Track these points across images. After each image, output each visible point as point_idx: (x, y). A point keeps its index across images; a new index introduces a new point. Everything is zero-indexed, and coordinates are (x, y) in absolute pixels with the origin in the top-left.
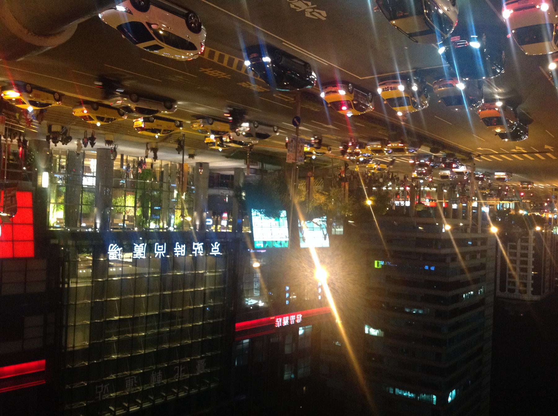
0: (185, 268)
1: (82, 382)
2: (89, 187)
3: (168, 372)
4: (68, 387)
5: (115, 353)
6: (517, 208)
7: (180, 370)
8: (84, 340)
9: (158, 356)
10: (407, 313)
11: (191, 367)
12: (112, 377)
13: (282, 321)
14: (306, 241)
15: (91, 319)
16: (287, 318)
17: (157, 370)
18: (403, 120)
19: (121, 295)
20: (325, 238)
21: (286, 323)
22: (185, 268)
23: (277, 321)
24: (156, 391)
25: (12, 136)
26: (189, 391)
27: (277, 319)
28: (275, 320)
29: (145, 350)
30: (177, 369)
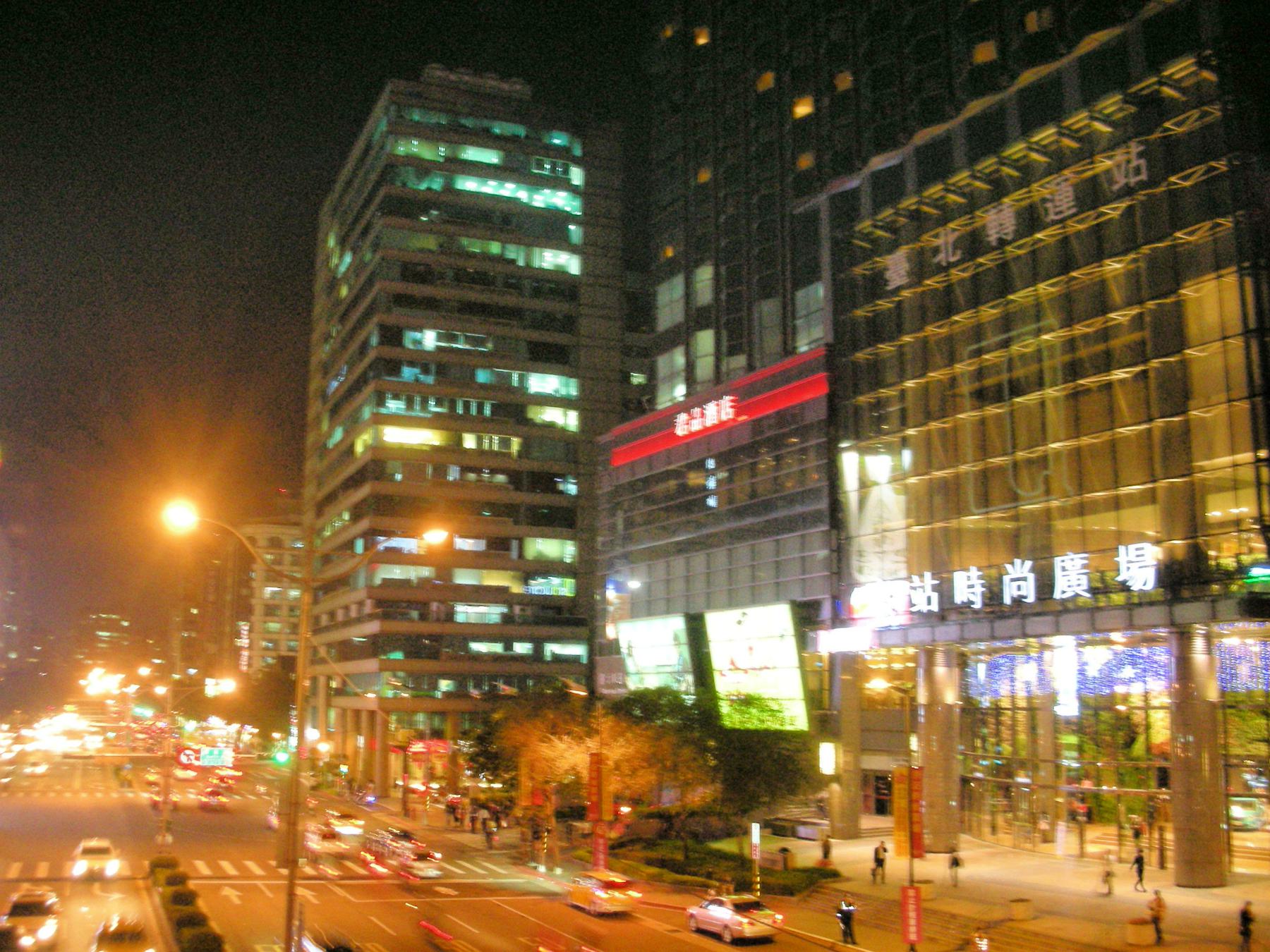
0: (1140, 871)
1: (1187, 184)
2: (1100, 636)
3: (973, 244)
4: (1221, 165)
5: (1115, 277)
6: (538, 651)
7: (947, 252)
8: (1199, 300)
9: (1003, 282)
10: (502, 472)
11: (921, 267)
12: (1114, 209)
13: (719, 412)
14: (671, 637)
15: (1184, 364)
16: (709, 423)
17: (1002, 243)
18: (1105, 342)
19: (1113, 445)
20: (630, 647)
21: (711, 408)
22: (1140, 871)
23: (731, 411)
24: (999, 189)
25: (590, 250)
26: (920, 203)
27: (731, 416)
28: (738, 414)
29: (1037, 297)
30: (954, 254)
